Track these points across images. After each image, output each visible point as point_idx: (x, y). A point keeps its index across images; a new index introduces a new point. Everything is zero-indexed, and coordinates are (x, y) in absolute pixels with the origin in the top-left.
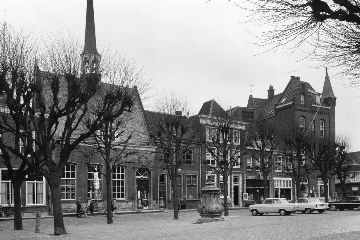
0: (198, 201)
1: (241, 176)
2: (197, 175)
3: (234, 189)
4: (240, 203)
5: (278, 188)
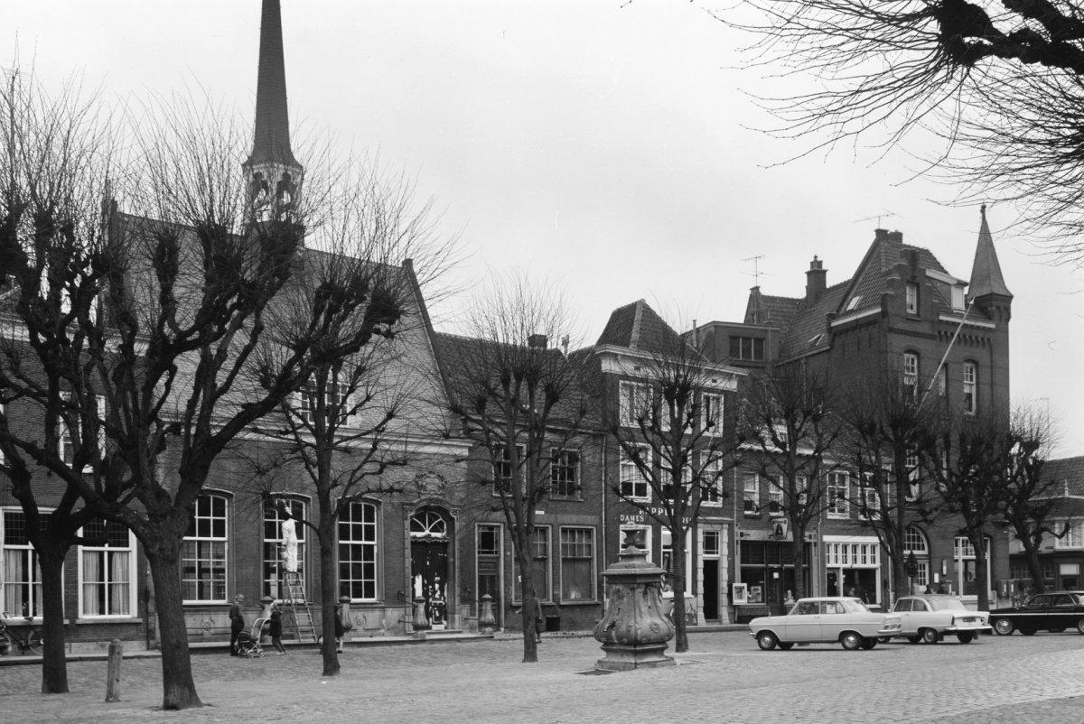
0: (596, 605)
1: (725, 532)
2: (592, 529)
3: (704, 570)
4: (724, 612)
5: (839, 568)
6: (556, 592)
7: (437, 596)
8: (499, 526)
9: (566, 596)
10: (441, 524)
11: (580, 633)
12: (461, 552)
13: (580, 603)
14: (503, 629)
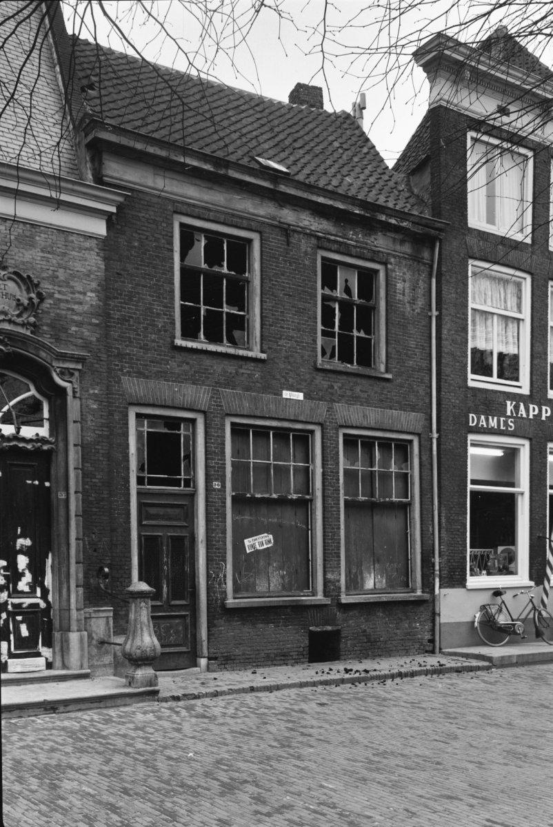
0: (419, 603)
2: (411, 442)
6: (329, 576)
7: (23, 586)
8: (193, 421)
9: (354, 583)
10: (34, 407)
11: (385, 666)
12: (86, 475)
13: (384, 598)
14: (203, 662)
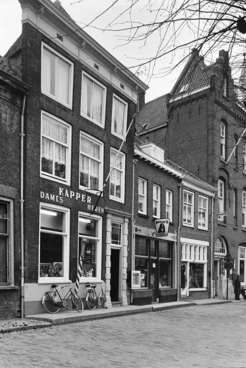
0: (13, 291)
1: (126, 225)
2: (9, 203)
3: (111, 256)
4: (124, 295)
5: (187, 262)
